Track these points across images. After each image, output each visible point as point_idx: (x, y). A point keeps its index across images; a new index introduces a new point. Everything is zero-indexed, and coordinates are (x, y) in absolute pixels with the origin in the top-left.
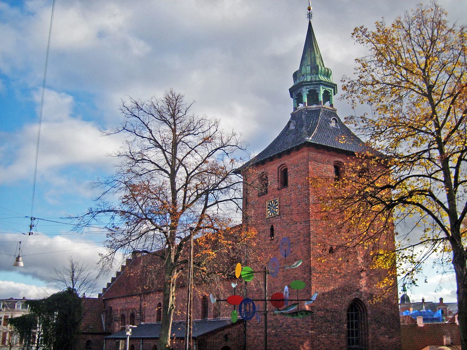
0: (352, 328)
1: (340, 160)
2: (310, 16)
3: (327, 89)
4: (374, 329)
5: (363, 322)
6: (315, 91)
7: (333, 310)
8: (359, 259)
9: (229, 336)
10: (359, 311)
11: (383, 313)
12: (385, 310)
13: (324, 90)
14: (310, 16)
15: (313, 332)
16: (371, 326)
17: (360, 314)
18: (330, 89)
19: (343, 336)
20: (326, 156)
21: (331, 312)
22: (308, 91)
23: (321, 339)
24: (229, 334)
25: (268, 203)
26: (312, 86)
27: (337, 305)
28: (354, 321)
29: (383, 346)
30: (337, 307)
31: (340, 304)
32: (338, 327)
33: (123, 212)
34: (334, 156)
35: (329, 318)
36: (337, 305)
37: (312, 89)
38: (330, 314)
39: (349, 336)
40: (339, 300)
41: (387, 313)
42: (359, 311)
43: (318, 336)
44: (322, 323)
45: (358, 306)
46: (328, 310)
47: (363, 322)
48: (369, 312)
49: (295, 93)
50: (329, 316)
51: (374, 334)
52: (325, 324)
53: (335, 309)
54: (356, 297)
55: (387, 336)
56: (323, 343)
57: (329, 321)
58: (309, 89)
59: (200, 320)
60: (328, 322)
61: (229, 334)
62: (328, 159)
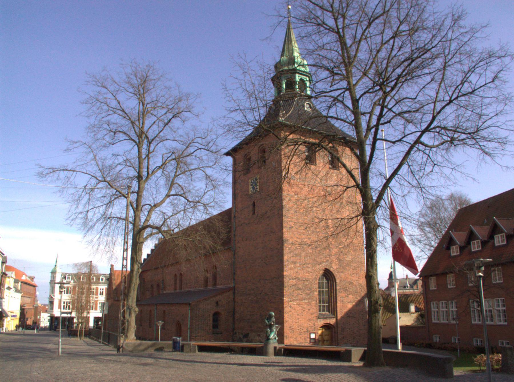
0: (323, 295)
3: (303, 77)
4: (342, 297)
7: (304, 279)
9: (219, 303)
11: (350, 283)
12: (352, 280)
13: (300, 78)
23: (292, 306)
24: (220, 301)
25: (250, 181)
27: (308, 275)
30: (308, 276)
31: (311, 274)
32: (308, 295)
33: (347, 239)
35: (300, 286)
36: (308, 275)
38: (301, 282)
39: (320, 303)
40: (310, 270)
41: (355, 283)
43: (290, 303)
44: (293, 291)
45: (329, 276)
46: (299, 279)
49: (276, 80)
50: (300, 284)
51: (343, 301)
52: (297, 292)
56: (295, 309)
57: (300, 289)
59: (202, 288)
61: (220, 301)
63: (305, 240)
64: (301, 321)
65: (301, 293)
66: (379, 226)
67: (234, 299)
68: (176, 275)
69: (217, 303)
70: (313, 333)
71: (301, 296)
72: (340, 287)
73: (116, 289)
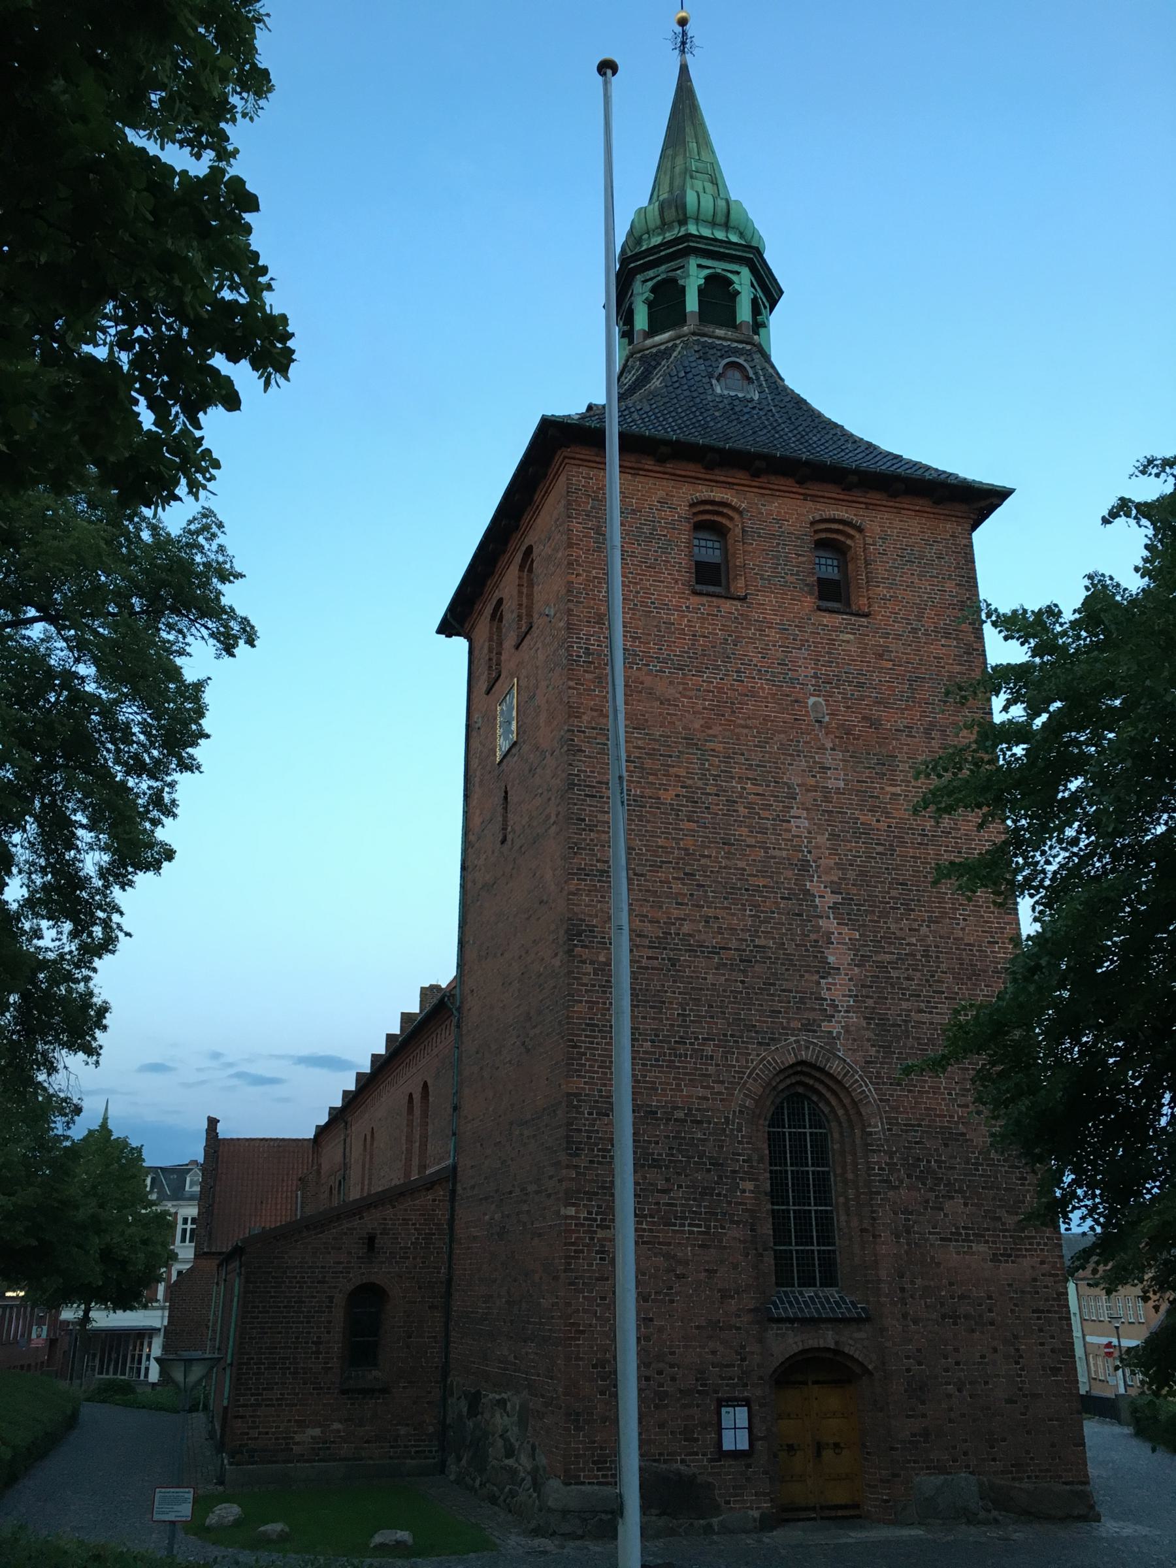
1: (718, 495)
2: (683, 45)
3: (720, 266)
5: (850, 1176)
6: (672, 282)
7: (679, 1114)
8: (815, 891)
10: (834, 1124)
14: (683, 45)
15: (571, 1211)
16: (891, 1193)
17: (836, 1136)
18: (735, 267)
19: (734, 1233)
20: (651, 481)
21: (669, 1120)
22: (653, 291)
26: (663, 268)
27: (701, 1092)
28: (789, 1168)
29: (962, 1297)
31: (718, 1088)
34: (694, 480)
36: (701, 1092)
37: (663, 276)
42: (834, 1124)
45: (828, 1103)
47: (850, 1176)
48: (877, 1127)
53: (690, 1110)
54: (804, 1055)
55: (981, 1248)
58: (655, 281)
60: (650, 1166)
62: (661, 493)
63: (686, 928)
64: (661, 1330)
65: (661, 1184)
66: (104, 1125)
67: (451, 1222)
68: (411, 1095)
69: (371, 1240)
70: (734, 1402)
71: (665, 1199)
72: (891, 1154)
73: (73, 844)
